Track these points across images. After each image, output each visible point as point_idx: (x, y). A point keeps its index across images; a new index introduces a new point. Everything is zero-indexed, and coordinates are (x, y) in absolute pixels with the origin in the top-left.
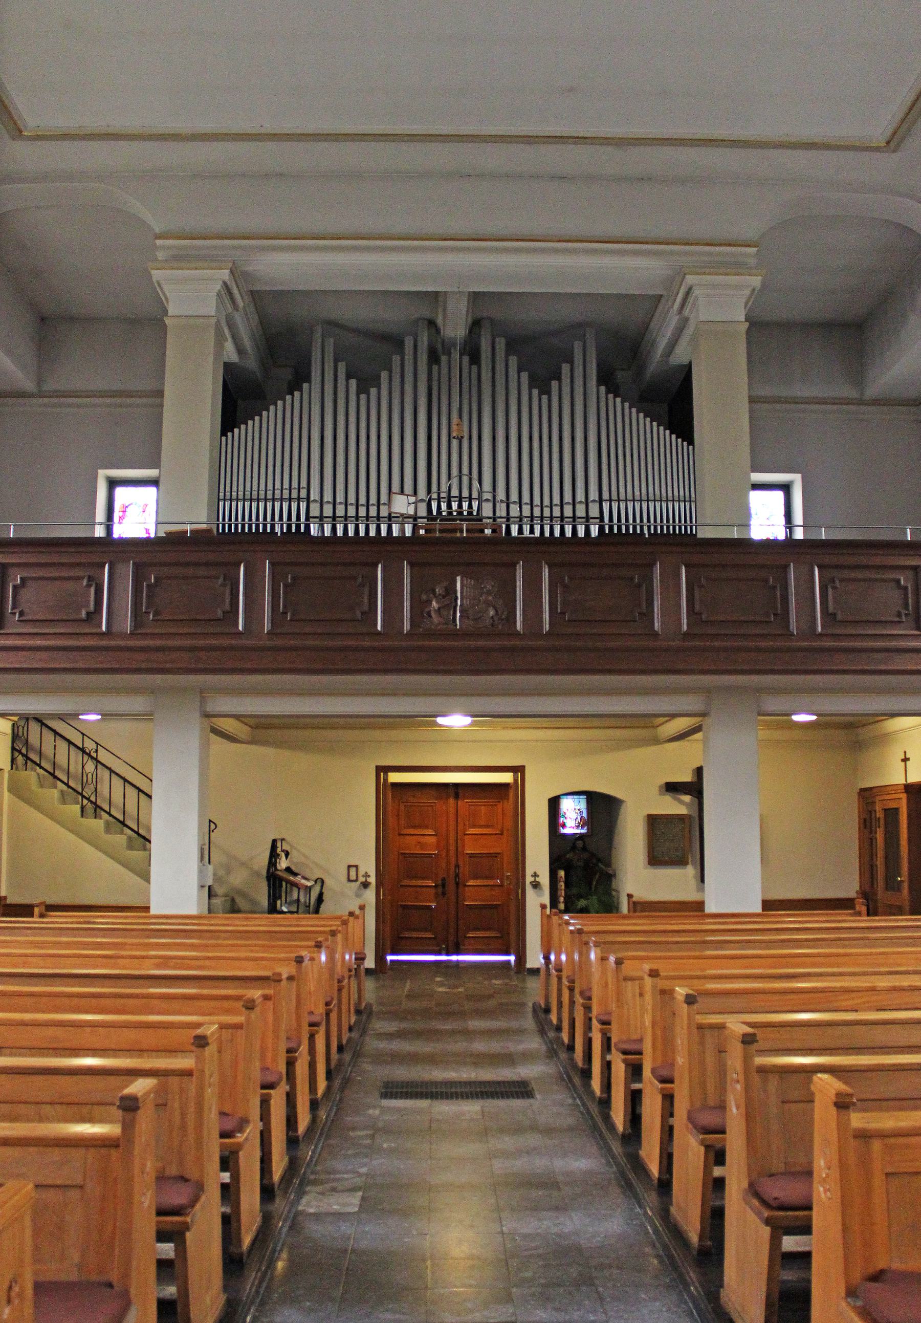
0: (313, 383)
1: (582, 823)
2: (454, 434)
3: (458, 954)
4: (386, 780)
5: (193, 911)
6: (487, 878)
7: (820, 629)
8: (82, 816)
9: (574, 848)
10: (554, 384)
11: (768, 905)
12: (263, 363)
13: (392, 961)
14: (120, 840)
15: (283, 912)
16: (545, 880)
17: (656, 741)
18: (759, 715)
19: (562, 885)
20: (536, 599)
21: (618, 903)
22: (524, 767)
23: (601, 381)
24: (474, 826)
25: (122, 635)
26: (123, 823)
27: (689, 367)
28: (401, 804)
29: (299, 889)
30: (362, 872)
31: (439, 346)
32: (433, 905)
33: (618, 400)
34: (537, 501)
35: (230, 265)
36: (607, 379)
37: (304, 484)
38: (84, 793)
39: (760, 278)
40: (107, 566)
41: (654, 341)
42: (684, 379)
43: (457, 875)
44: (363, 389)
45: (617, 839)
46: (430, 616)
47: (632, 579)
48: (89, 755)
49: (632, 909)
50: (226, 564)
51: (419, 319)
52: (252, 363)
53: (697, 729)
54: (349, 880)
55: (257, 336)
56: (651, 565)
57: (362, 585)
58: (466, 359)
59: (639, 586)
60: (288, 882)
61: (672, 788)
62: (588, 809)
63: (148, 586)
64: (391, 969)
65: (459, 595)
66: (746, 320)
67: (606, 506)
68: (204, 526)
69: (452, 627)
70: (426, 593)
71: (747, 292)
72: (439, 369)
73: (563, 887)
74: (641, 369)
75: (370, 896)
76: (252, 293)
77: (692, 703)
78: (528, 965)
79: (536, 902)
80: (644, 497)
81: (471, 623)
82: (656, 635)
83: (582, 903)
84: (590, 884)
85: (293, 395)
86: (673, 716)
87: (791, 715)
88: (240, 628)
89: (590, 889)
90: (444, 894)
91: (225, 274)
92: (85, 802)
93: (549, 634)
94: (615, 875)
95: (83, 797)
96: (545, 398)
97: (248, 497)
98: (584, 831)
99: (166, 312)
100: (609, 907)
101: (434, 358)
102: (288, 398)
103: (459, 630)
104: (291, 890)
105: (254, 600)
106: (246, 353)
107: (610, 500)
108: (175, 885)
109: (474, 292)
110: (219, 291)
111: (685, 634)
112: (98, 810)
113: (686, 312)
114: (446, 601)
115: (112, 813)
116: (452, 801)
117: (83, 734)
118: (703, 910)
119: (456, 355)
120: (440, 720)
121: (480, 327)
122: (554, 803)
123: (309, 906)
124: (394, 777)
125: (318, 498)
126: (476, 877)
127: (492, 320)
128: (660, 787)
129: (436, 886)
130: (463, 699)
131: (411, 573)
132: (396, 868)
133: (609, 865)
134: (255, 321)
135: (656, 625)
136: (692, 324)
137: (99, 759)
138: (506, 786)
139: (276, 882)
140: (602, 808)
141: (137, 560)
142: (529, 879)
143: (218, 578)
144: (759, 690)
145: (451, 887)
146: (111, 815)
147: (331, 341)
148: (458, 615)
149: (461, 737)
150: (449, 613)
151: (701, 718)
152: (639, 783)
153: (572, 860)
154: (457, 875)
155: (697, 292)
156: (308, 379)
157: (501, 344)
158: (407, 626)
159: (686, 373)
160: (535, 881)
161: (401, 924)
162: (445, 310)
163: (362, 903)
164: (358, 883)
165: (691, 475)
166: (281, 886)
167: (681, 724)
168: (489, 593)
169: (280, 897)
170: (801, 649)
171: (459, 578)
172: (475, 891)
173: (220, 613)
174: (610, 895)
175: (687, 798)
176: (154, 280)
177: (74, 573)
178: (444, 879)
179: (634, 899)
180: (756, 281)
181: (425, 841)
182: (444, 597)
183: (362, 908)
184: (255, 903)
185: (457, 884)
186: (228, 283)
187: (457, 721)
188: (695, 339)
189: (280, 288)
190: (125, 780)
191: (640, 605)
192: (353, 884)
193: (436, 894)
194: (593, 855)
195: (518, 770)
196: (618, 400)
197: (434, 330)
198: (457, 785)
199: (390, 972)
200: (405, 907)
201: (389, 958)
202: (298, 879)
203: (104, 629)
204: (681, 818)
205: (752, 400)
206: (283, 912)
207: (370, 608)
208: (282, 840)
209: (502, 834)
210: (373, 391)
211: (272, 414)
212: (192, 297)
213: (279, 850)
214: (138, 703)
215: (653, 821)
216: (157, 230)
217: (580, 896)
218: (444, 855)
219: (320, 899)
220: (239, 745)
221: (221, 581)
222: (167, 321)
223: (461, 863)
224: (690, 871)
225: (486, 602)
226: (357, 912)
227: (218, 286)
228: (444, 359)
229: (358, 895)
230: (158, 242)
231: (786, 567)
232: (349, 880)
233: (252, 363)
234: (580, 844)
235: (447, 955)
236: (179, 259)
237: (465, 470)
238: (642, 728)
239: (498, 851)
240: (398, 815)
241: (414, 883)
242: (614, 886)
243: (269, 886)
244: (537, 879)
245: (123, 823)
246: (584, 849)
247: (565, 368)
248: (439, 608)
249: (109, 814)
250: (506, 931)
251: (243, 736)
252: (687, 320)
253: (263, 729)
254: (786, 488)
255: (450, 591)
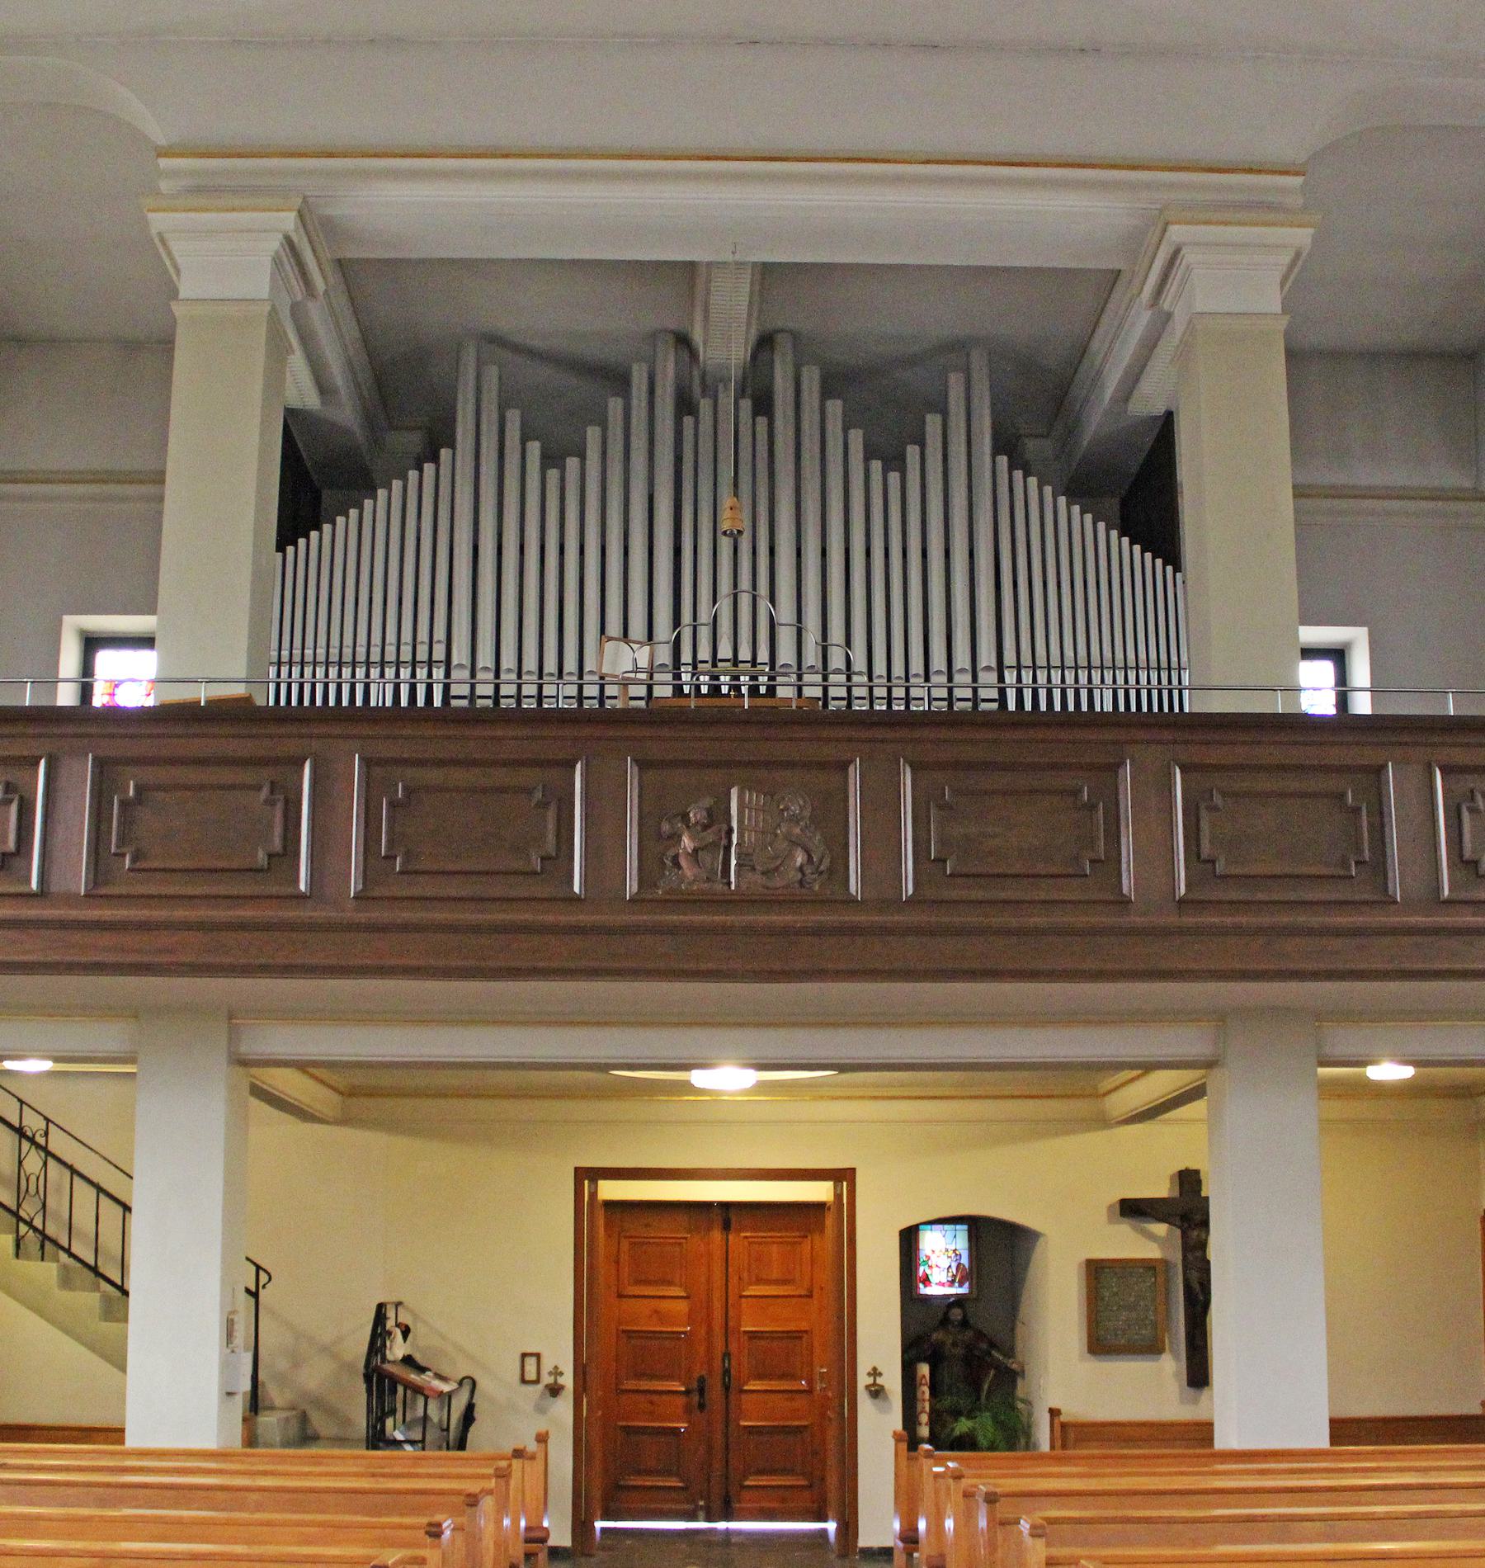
0: (459, 447)
1: (961, 1276)
2: (725, 525)
3: (728, 1518)
4: (593, 1195)
5: (211, 1444)
6: (782, 1377)
7: (1446, 892)
8: (17, 1256)
9: (945, 1321)
10: (912, 452)
11: (1343, 1430)
12: (369, 421)
13: (603, 1530)
14: (88, 1300)
15: (397, 1444)
16: (893, 1381)
17: (1103, 1122)
18: (1322, 1064)
19: (925, 1391)
20: (887, 839)
21: (1029, 1427)
22: (853, 1170)
23: (996, 451)
24: (759, 1281)
25: (70, 899)
26: (94, 1270)
27: (1169, 418)
28: (622, 1242)
29: (427, 1398)
30: (547, 1366)
31: (697, 389)
32: (682, 1426)
33: (1033, 481)
34: (880, 668)
35: (298, 202)
36: (1006, 444)
37: (440, 634)
38: (22, 1213)
39: (1311, 231)
40: (43, 763)
41: (1099, 373)
42: (1158, 440)
43: (726, 1372)
44: (552, 459)
45: (1024, 1311)
46: (679, 867)
47: (1076, 792)
48: (32, 1141)
49: (1058, 1444)
50: (275, 761)
51: (653, 336)
52: (346, 414)
53: (1195, 1093)
54: (524, 1381)
55: (351, 353)
56: (1115, 768)
57: (543, 805)
58: (746, 405)
59: (1091, 807)
60: (408, 1385)
61: (1133, 1209)
62: (970, 1249)
63: (122, 803)
64: (603, 1549)
65: (735, 825)
66: (1284, 312)
67: (1010, 677)
68: (239, 690)
69: (719, 887)
70: (669, 820)
71: (1286, 258)
72: (697, 423)
73: (927, 1396)
74: (1072, 432)
75: (564, 1409)
76: (340, 263)
77: (1190, 1041)
78: (864, 1542)
79: (878, 1428)
80: (1083, 662)
81: (758, 878)
82: (1125, 902)
83: (963, 1426)
84: (977, 1389)
85: (421, 470)
86: (1148, 1067)
87: (1363, 1064)
88: (302, 887)
89: (978, 1399)
90: (702, 1406)
91: (288, 221)
92: (23, 1228)
93: (909, 901)
94: (1022, 1373)
95: (20, 1219)
96: (894, 477)
97: (334, 657)
98: (964, 1290)
99: (174, 293)
100: (1013, 1435)
101: (685, 405)
102: (413, 475)
103: (733, 893)
104: (414, 1401)
105: (330, 838)
106: (336, 392)
107: (1089, 668)
108: (174, 1389)
109: (765, 265)
110: (277, 252)
111: (1181, 901)
112: (47, 1244)
113: (1166, 304)
114: (709, 836)
115: (74, 1250)
116: (717, 1235)
117: (22, 1102)
118: (1209, 1440)
119: (727, 399)
120: (698, 1078)
121: (772, 349)
122: (909, 1239)
123: (448, 1429)
124: (610, 1190)
125: (466, 661)
126: (760, 1377)
127: (795, 336)
128: (1110, 1207)
129: (687, 1392)
130: (736, 1034)
131: (640, 778)
132: (613, 1360)
133: (1010, 1352)
134: (352, 331)
135: (1125, 881)
136: (1178, 326)
137: (51, 1147)
138: (820, 1207)
139: (384, 1383)
140: (998, 1245)
141: (100, 753)
142: (863, 1380)
143: (259, 788)
144: (1320, 1016)
145: (715, 1392)
146: (68, 1252)
147: (492, 374)
148: (733, 862)
149: (737, 1109)
150: (715, 858)
151: (1203, 1072)
152: (1073, 1196)
153: (943, 1343)
154: (726, 1372)
155: (1189, 256)
156: (452, 445)
157: (812, 378)
158: (632, 886)
159: (1164, 432)
160: (875, 1384)
161: (619, 1462)
162: (706, 311)
163: (542, 1428)
164: (540, 1387)
165: (1167, 623)
166: (394, 1392)
167: (1162, 1084)
168: (795, 820)
169: (393, 1412)
170: (1411, 931)
171: (734, 792)
172: (760, 1403)
173: (261, 857)
174: (1013, 1408)
175: (1161, 1229)
176: (154, 232)
177: (247, 776)
178: (702, 1380)
179: (1063, 1418)
180: (1302, 236)
181: (671, 1308)
182: (705, 827)
183: (542, 1439)
184: (347, 1422)
185: (727, 1388)
186: (295, 239)
187: (727, 1079)
188: (1185, 352)
189: (392, 255)
190: (100, 1189)
191: (1093, 841)
192: (531, 1388)
193: (688, 1409)
194: (980, 1335)
195: (843, 1176)
196: (1033, 481)
197: (686, 355)
198: (726, 1206)
199: (601, 1555)
200: (627, 1430)
201: (599, 1524)
202: (426, 1379)
203: (34, 885)
204: (1149, 1266)
205: (1301, 492)
206: (397, 1444)
207: (558, 848)
208: (398, 1304)
209: (810, 1296)
210: (572, 463)
211: (380, 505)
212: (223, 264)
213: (390, 1324)
214: (109, 1036)
215: (1096, 1271)
216: (162, 141)
217: (956, 1414)
218: (703, 1332)
219: (469, 1417)
220: (316, 1126)
221: (265, 793)
222: (178, 309)
223: (733, 1347)
224: (1170, 1366)
225: (788, 837)
226: (532, 1446)
227: (274, 244)
228: (705, 406)
229: (541, 1409)
230: (164, 163)
231: (1380, 770)
232: (524, 1381)
233: (346, 414)
234: (956, 1314)
235: (708, 1520)
236: (205, 192)
237: (745, 583)
238: (1071, 1092)
239: (804, 1326)
240: (617, 1262)
241: (645, 1385)
242: (1020, 1392)
243: (369, 1391)
244: (879, 1381)
245: (94, 1270)
246: (965, 1323)
247: (933, 422)
248: (696, 851)
249: (68, 1252)
250: (827, 1483)
251: (327, 1111)
252: (1169, 316)
253: (366, 1096)
254: (1338, 655)
255: (718, 816)
